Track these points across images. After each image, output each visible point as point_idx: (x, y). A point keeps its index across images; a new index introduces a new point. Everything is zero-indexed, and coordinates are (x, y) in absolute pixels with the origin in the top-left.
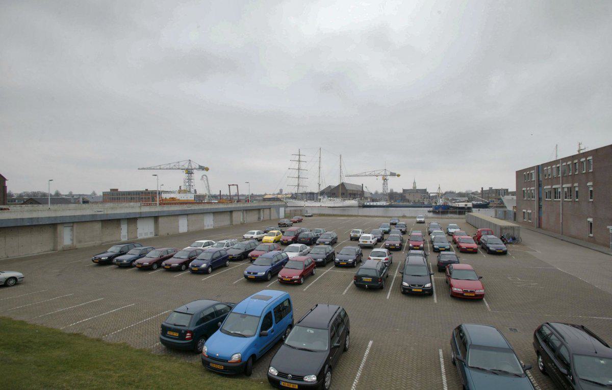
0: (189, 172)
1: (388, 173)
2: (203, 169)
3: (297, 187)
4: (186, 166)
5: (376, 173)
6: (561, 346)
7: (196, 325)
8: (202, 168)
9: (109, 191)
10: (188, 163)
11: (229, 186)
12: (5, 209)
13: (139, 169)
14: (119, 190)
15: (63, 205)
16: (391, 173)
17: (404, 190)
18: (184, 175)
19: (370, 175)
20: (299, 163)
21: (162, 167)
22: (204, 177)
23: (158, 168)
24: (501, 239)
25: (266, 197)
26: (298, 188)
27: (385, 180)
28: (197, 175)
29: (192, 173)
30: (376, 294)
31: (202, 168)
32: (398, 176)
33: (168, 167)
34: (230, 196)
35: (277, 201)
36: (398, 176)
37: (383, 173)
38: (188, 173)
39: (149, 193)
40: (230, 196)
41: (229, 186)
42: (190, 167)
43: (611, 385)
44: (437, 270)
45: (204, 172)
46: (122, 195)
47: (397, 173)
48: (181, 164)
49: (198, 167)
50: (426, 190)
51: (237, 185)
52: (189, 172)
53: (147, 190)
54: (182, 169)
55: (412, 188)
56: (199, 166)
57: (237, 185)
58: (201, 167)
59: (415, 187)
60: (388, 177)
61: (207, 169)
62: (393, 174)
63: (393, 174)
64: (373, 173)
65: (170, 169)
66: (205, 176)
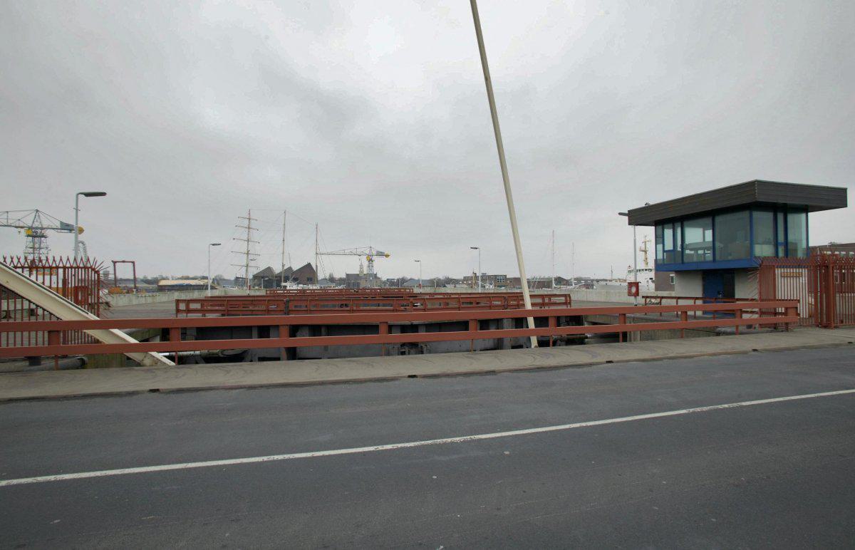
1: (374, 253)
3: (244, 269)
5: (359, 251)
6: (57, 363)
10: (34, 214)
11: (115, 263)
12: (179, 279)
15: (710, 209)
17: (347, 275)
22: (80, 245)
24: (775, 324)
25: (163, 283)
27: (370, 261)
30: (130, 370)
34: (135, 280)
35: (187, 289)
36: (387, 256)
37: (367, 252)
38: (34, 237)
40: (135, 280)
41: (115, 263)
42: (36, 224)
44: (298, 350)
50: (376, 274)
51: (133, 263)
54: (16, 227)
56: (62, 223)
57: (133, 263)
58: (68, 225)
59: (361, 272)
60: (374, 258)
62: (380, 254)
63: (380, 254)
64: (354, 251)
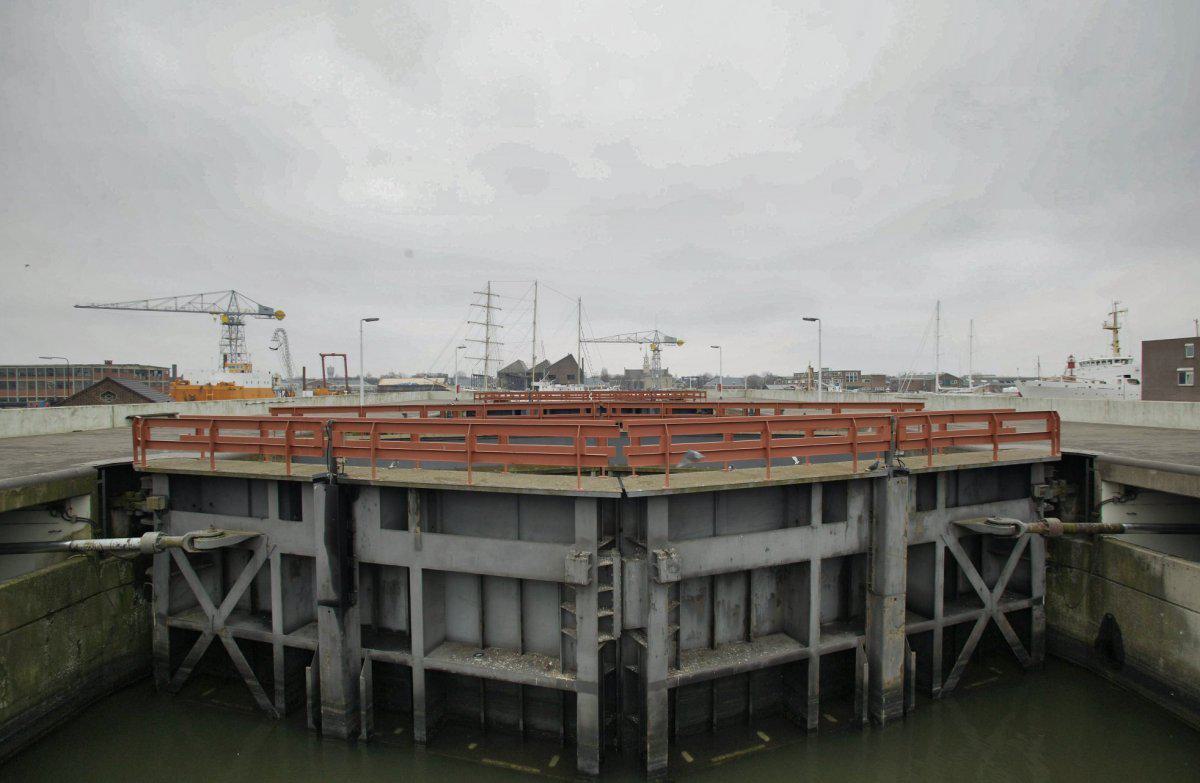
0: (232, 321)
1: (662, 339)
2: (270, 315)
3: (483, 362)
4: (224, 306)
5: (640, 336)
7: (238, 640)
8: (266, 312)
9: (103, 363)
11: (323, 356)
13: (77, 306)
14: (591, 370)
16: (666, 337)
18: (217, 329)
19: (629, 341)
20: (488, 312)
21: (151, 305)
22: (280, 333)
23: (141, 305)
26: (486, 365)
27: (656, 350)
28: (257, 332)
29: (240, 324)
31: (266, 312)
32: (680, 343)
33: (171, 304)
34: (347, 379)
36: (680, 343)
37: (652, 337)
38: (230, 324)
39: (116, 371)
41: (323, 356)
42: (233, 309)
43: (3, 406)
45: (274, 323)
46: (23, 375)
47: (679, 339)
48: (213, 299)
49: (257, 310)
51: (344, 356)
52: (232, 321)
53: (108, 363)
54: (211, 313)
55: (641, 368)
57: (344, 356)
58: (267, 309)
60: (662, 346)
61: (280, 316)
62: (670, 341)
63: (670, 341)
65: (176, 311)
66: (283, 331)
